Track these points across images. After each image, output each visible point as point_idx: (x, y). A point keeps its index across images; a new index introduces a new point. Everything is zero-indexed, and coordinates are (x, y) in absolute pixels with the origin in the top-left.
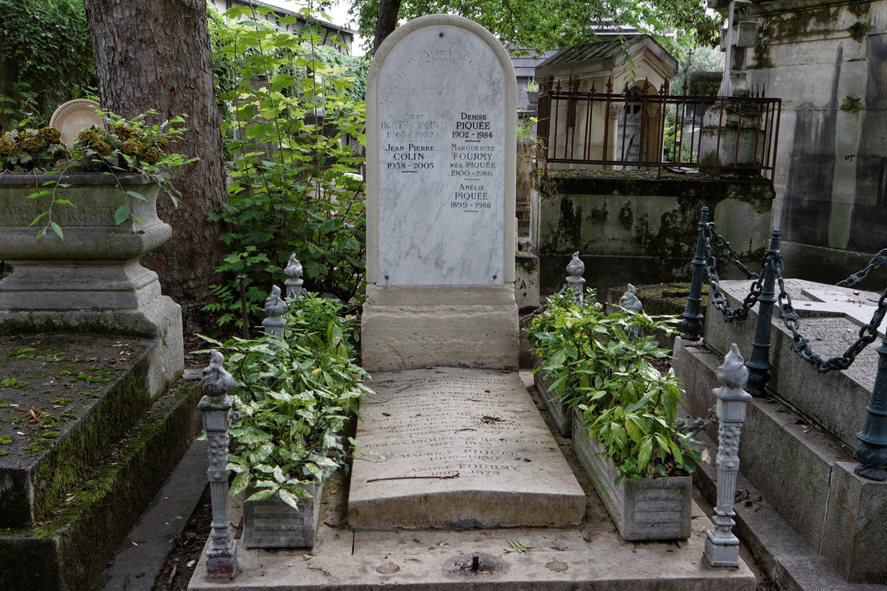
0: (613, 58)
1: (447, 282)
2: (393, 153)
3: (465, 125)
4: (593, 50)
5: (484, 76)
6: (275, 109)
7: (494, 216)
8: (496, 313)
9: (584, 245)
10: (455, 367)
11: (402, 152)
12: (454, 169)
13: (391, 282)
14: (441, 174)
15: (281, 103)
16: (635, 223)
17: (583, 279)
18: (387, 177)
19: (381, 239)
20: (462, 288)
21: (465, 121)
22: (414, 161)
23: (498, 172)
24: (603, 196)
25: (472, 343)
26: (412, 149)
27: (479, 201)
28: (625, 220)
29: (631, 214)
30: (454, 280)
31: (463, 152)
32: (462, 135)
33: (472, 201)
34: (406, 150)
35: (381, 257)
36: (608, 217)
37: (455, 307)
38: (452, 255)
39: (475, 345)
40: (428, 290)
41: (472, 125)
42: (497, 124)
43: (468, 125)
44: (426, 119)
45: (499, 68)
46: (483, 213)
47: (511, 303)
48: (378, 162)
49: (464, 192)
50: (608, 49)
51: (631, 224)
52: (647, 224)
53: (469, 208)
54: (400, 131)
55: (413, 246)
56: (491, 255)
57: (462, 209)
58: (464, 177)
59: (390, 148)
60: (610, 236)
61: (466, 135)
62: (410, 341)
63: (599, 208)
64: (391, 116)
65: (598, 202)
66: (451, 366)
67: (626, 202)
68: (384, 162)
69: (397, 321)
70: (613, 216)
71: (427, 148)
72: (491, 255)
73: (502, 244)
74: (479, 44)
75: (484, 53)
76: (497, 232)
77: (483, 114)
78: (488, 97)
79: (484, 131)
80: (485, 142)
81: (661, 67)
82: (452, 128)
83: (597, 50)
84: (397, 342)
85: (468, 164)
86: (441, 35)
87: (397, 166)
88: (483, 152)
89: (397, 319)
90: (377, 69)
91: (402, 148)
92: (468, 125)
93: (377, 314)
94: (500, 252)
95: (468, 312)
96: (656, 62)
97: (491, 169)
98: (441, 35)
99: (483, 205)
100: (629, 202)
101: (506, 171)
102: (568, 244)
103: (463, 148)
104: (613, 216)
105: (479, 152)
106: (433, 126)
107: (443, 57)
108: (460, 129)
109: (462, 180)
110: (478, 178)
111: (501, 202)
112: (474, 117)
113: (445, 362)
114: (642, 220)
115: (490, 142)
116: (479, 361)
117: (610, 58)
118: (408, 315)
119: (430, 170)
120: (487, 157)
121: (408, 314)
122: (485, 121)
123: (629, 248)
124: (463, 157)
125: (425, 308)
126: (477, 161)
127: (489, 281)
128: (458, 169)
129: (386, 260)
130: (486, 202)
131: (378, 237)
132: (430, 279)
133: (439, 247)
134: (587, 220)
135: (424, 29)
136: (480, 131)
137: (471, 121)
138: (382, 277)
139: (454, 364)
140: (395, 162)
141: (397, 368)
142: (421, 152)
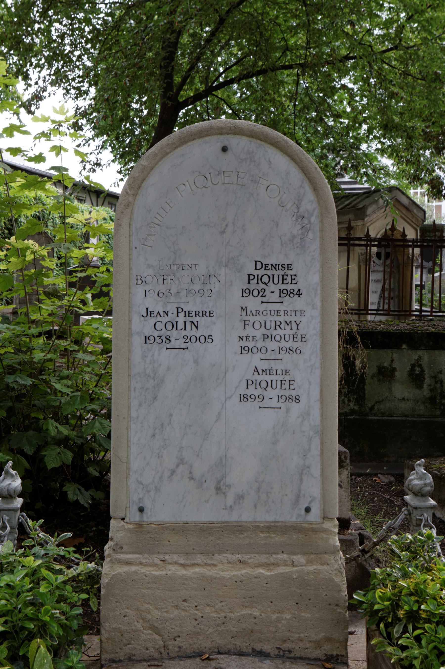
0: (364, 209)
1: (234, 517)
2: (152, 321)
3: (260, 279)
4: (343, 203)
5: (289, 206)
6: (21, 259)
7: (305, 415)
8: (311, 568)
9: (370, 406)
10: (247, 655)
11: (166, 319)
12: (243, 343)
13: (148, 517)
14: (223, 350)
15: (28, 252)
16: (427, 381)
17: (432, 502)
18: (144, 357)
19: (134, 449)
20: (256, 528)
21: (260, 273)
22: (184, 333)
23: (311, 348)
24: (389, 351)
25: (274, 617)
26: (182, 315)
27: (282, 393)
28: (416, 377)
29: (422, 371)
30: (246, 515)
31: (258, 318)
32: (256, 293)
33: (272, 393)
34: (172, 317)
35: (133, 478)
36: (397, 374)
37: (246, 557)
38: (242, 475)
39: (278, 620)
40: (206, 530)
41: (271, 278)
42: (309, 276)
43: (265, 279)
44: (202, 270)
45: (310, 195)
46: (288, 410)
47: (334, 552)
48: (130, 335)
49: (259, 378)
50: (358, 201)
51: (423, 382)
52: (441, 382)
53: (267, 402)
54: (163, 288)
55: (181, 461)
56: (301, 474)
57: (256, 404)
58: (259, 355)
59: (149, 313)
60: (399, 396)
61: (262, 293)
62: (176, 612)
63: (385, 364)
64: (149, 266)
65: (385, 357)
66: (241, 654)
67: (417, 357)
68: (138, 333)
69: (156, 580)
70: (401, 374)
71: (204, 314)
72: (301, 474)
73: (318, 458)
74: (281, 161)
75: (288, 174)
76: (310, 440)
77: (286, 262)
78: (294, 237)
79: (289, 287)
80: (290, 303)
81: (409, 215)
82: (240, 284)
83: (347, 203)
84: (156, 613)
85: (265, 337)
86: (224, 149)
87: (158, 340)
88: (288, 319)
89: (156, 577)
90: (131, 199)
91: (166, 313)
92: (265, 279)
93: (126, 569)
94: (316, 471)
95: (267, 565)
96: (404, 211)
97: (299, 344)
98: (224, 149)
99: (288, 399)
100: (420, 357)
101: (323, 347)
102: (351, 404)
103: (258, 313)
104: (401, 374)
105: (282, 319)
106: (213, 279)
107: (227, 180)
108: (253, 285)
109: (256, 359)
110: (280, 357)
111: (315, 393)
112: (274, 267)
113: (231, 647)
114: (435, 377)
115: (298, 303)
116: (286, 646)
117: (361, 208)
118: (172, 570)
119: (209, 346)
120: (294, 325)
121: (173, 568)
122: (290, 273)
123: (422, 409)
124: (257, 325)
125: (199, 559)
126: (279, 332)
127: (299, 515)
128: (251, 344)
129: (140, 483)
130: (294, 393)
131: (129, 447)
132: (208, 512)
133: (222, 463)
134: (372, 377)
135: (200, 141)
136: (283, 287)
137: (269, 273)
138: (135, 509)
139: (245, 650)
140: (156, 334)
141: (156, 655)
142: (195, 320)
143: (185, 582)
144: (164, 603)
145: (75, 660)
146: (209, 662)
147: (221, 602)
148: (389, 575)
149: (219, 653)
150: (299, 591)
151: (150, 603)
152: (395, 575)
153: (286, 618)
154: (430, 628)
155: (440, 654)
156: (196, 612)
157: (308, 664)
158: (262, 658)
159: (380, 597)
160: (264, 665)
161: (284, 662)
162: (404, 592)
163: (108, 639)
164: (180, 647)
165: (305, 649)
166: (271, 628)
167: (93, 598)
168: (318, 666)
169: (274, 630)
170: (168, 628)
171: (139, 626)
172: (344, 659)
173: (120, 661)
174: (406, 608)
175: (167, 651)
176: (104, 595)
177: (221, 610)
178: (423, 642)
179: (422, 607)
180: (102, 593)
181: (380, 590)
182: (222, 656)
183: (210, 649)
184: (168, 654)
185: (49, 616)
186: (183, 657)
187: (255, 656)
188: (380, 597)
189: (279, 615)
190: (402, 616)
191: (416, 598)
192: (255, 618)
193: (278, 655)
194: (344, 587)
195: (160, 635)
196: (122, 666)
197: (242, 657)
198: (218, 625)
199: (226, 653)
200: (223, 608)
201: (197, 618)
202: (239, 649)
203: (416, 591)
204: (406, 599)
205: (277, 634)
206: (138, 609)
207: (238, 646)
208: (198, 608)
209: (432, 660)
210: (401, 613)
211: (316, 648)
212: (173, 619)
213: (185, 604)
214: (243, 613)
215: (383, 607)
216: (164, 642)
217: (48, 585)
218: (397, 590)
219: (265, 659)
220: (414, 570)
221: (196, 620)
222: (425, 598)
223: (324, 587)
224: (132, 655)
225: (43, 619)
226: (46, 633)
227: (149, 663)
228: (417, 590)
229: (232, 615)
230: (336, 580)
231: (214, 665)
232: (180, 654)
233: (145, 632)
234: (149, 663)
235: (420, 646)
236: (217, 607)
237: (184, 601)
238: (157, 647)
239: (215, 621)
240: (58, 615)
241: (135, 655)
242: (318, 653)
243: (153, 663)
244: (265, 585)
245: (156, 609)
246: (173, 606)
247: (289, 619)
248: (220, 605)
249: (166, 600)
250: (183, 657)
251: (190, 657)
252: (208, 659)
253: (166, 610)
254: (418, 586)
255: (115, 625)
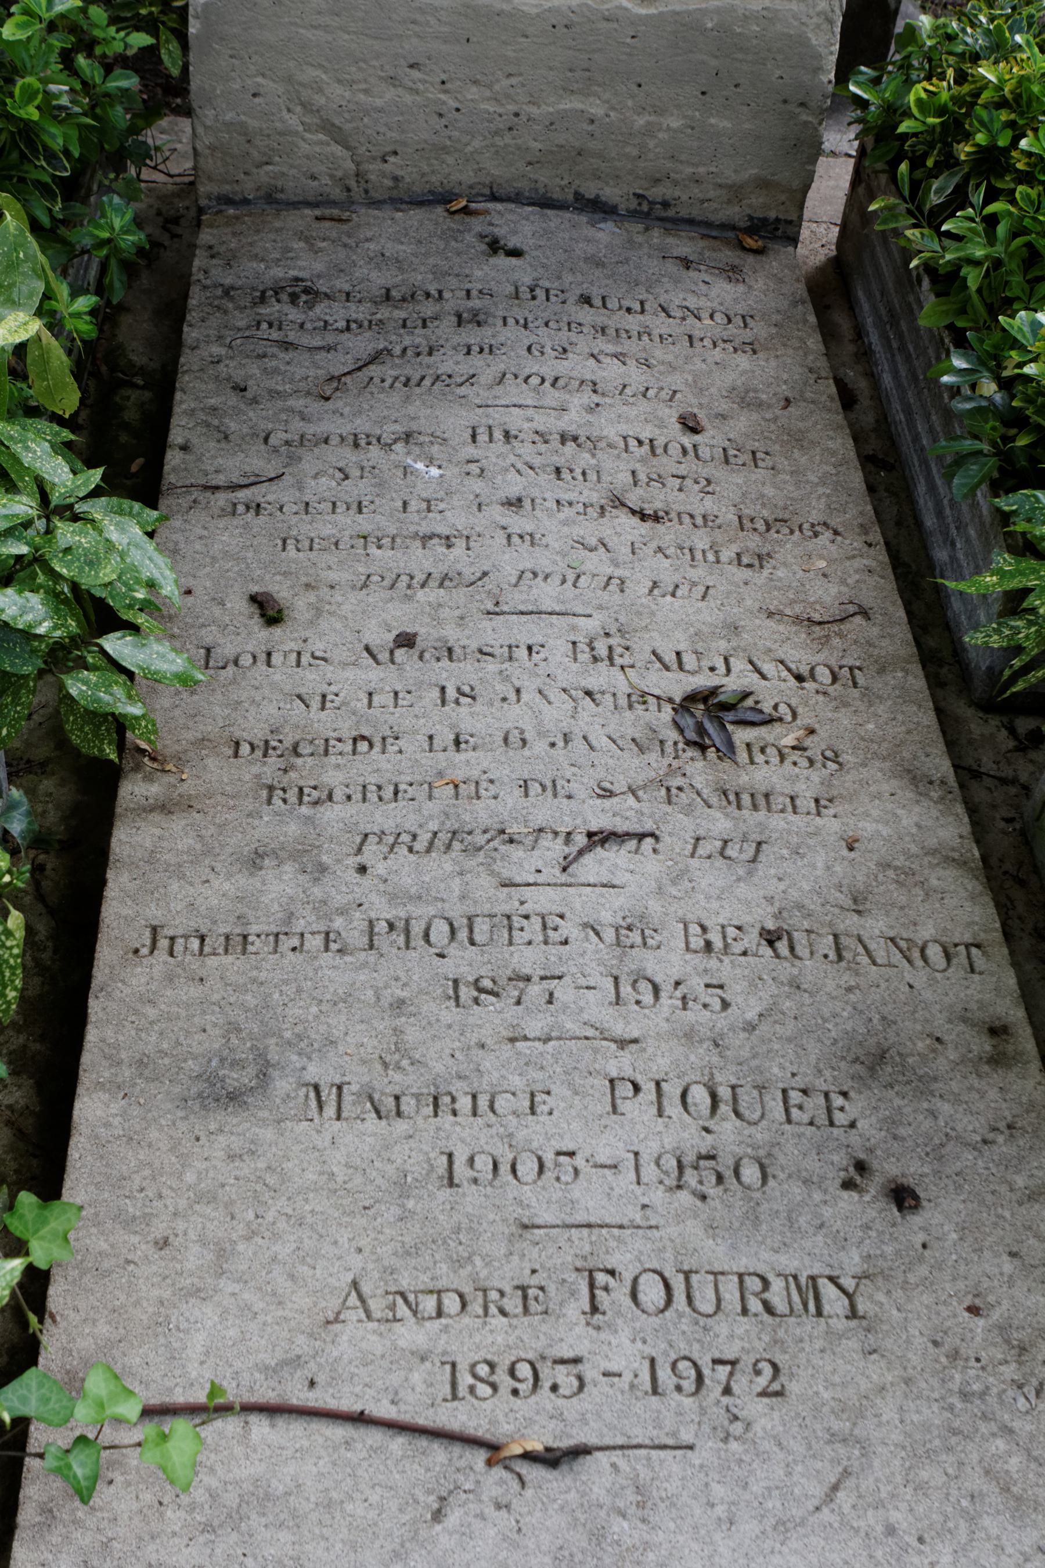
25: (641, 121)
39: (649, 131)
62: (390, 94)
66: (546, 203)
84: (338, 93)
113: (522, 185)
116: (657, 193)
139: (557, 195)
141: (337, 193)
143: (418, 17)
144: (360, 69)
145: (117, 223)
146: (467, 219)
147: (510, 75)
148: (950, 38)
149: (494, 198)
150: (714, 63)
151: (321, 66)
152: (969, 40)
153: (669, 128)
154: (1028, 195)
155: (1032, 257)
156: (442, 96)
157: (704, 236)
158: (597, 216)
159: (919, 101)
160: (600, 235)
161: (647, 229)
162: (985, 96)
163: (212, 148)
164: (396, 179)
165: (702, 202)
166: (628, 150)
167: (167, 41)
168: (727, 242)
169: (635, 152)
170: (369, 131)
171: (293, 121)
172: (791, 230)
173: (246, 202)
174: (981, 138)
175: (363, 184)
176: (197, 37)
177: (508, 96)
178: (1001, 230)
179: (1023, 143)
180: (192, 30)
181: (925, 84)
182: (499, 206)
183: (471, 187)
184: (366, 192)
185: (38, 108)
186: (402, 201)
187: (581, 210)
188: (919, 101)
189: (652, 118)
190: (963, 157)
191: (1013, 116)
192: (592, 121)
193: (635, 211)
194: (831, 62)
195: (348, 148)
196: (250, 215)
197: (549, 212)
198: (496, 133)
199: (509, 200)
200: (511, 91)
201: (444, 110)
202: (542, 191)
203: (1018, 97)
204: (984, 114)
205: (642, 164)
206: (289, 79)
207: (540, 185)
208: (448, 86)
209: (1011, 272)
210: (964, 150)
211: (729, 202)
212: (380, 111)
213: (416, 74)
214: (562, 106)
215: (922, 128)
216: (358, 164)
217: (25, 18)
218: (966, 88)
219: (605, 220)
220: (1028, 43)
221: (441, 115)
222: (1035, 118)
223: (779, 57)
224: (276, 189)
225: (22, 114)
226: (35, 151)
227: (318, 212)
228: (1020, 95)
229: (534, 111)
230: (814, 42)
231: (479, 229)
232: (395, 194)
233: (308, 136)
234: (318, 212)
235: (991, 239)
236: (497, 87)
237: (411, 66)
238: (339, 174)
239: (490, 121)
240: (64, 101)
241: (282, 191)
242: (734, 213)
243: (328, 212)
244: (629, 40)
245: (339, 81)
246: (381, 78)
247: (675, 131)
248: (506, 82)
249: (365, 61)
250: (402, 201)
251: (421, 204)
252: (465, 211)
253: (363, 86)
254: (1026, 84)
255: (229, 116)
